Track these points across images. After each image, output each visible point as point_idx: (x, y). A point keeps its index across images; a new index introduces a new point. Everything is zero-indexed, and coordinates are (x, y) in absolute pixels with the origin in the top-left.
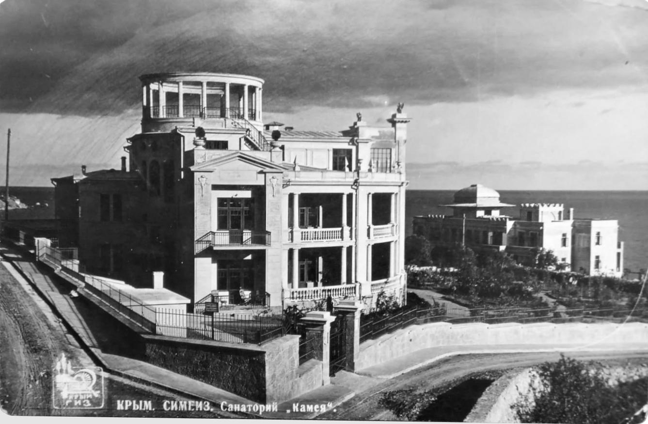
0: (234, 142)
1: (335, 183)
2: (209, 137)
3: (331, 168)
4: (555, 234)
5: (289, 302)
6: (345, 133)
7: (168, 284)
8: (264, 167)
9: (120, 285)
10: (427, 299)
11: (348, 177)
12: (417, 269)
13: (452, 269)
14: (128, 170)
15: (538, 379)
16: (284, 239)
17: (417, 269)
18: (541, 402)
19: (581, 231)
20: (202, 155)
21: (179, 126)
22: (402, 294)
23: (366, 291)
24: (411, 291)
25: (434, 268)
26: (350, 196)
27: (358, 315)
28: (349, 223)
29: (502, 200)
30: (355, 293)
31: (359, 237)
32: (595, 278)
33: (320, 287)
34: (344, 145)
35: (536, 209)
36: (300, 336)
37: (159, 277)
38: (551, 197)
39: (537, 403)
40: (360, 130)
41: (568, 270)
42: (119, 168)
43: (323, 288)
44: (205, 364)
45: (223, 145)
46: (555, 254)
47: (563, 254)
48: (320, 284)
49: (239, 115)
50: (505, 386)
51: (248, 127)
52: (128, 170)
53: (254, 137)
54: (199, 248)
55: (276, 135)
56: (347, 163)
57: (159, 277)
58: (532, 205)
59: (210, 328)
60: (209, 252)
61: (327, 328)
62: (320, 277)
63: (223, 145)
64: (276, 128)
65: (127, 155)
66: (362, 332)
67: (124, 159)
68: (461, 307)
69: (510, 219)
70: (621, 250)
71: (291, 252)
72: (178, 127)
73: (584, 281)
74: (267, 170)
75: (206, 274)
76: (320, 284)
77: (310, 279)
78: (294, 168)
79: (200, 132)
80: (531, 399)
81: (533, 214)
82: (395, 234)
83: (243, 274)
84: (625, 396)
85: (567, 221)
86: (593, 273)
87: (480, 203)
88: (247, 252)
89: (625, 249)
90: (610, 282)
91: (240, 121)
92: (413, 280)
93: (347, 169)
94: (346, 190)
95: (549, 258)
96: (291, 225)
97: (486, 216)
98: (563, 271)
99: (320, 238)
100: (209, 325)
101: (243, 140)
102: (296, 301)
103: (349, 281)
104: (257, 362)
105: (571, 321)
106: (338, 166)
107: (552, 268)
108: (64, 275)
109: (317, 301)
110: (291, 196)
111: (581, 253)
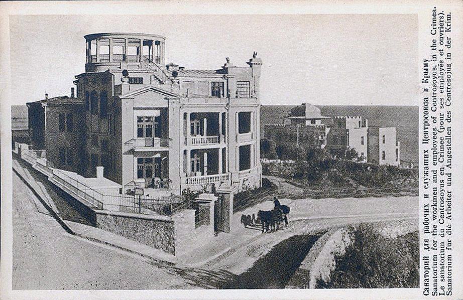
0: (146, 78)
1: (215, 106)
2: (130, 75)
3: (211, 95)
4: (357, 140)
5: (184, 186)
6: (218, 72)
7: (106, 175)
8: (168, 96)
9: (74, 175)
10: (275, 183)
11: (224, 101)
12: (268, 162)
13: (291, 161)
14: (76, 97)
15: (347, 236)
16: (181, 142)
17: (268, 162)
18: (349, 250)
19: (373, 132)
20: (127, 90)
21: (111, 68)
22: (259, 179)
23: (235, 178)
24: (264, 177)
25: (279, 161)
26: (224, 114)
27: (232, 197)
28: (224, 133)
29: (322, 114)
30: (228, 179)
31: (231, 144)
32: (382, 167)
33: (206, 176)
34: (219, 78)
35: (344, 120)
36: (196, 210)
37: (100, 170)
38: (354, 111)
39: (347, 251)
40: (229, 70)
41: (365, 161)
42: (69, 96)
43: (145, 126)
44: (135, 230)
45: (140, 81)
46: (357, 151)
47: (362, 150)
48: (206, 174)
49: (149, 59)
50: (326, 241)
51: (156, 68)
52: (76, 97)
53: (160, 74)
54: (125, 149)
55: (175, 74)
56: (222, 93)
57: (100, 170)
58: (342, 117)
59: (138, 206)
60: (132, 152)
61: (212, 205)
62: (206, 169)
63: (140, 81)
64: (174, 68)
65: (75, 87)
66: (234, 207)
67: (73, 89)
68: (296, 188)
69: (328, 127)
70: (398, 147)
71: (185, 152)
72: (110, 69)
73: (375, 169)
74: (170, 97)
75: (129, 166)
76: (206, 174)
77: (158, 134)
78: (187, 96)
79: (125, 73)
80: (343, 248)
81: (342, 123)
82: (253, 139)
83: (154, 169)
84: (401, 245)
85: (364, 128)
86: (382, 162)
87: (307, 116)
88: (156, 153)
89: (401, 146)
90: (391, 169)
91: (150, 64)
92: (266, 170)
93: (222, 96)
94: (221, 111)
95: (353, 153)
96: (185, 134)
97: (312, 125)
98: (362, 162)
99: (203, 143)
100: (137, 204)
101: (153, 77)
102: (189, 185)
103: (224, 172)
104: (168, 226)
105: (367, 196)
106: (216, 93)
107: (355, 160)
108: (38, 169)
109: (203, 186)
110: (185, 114)
111: (373, 150)
